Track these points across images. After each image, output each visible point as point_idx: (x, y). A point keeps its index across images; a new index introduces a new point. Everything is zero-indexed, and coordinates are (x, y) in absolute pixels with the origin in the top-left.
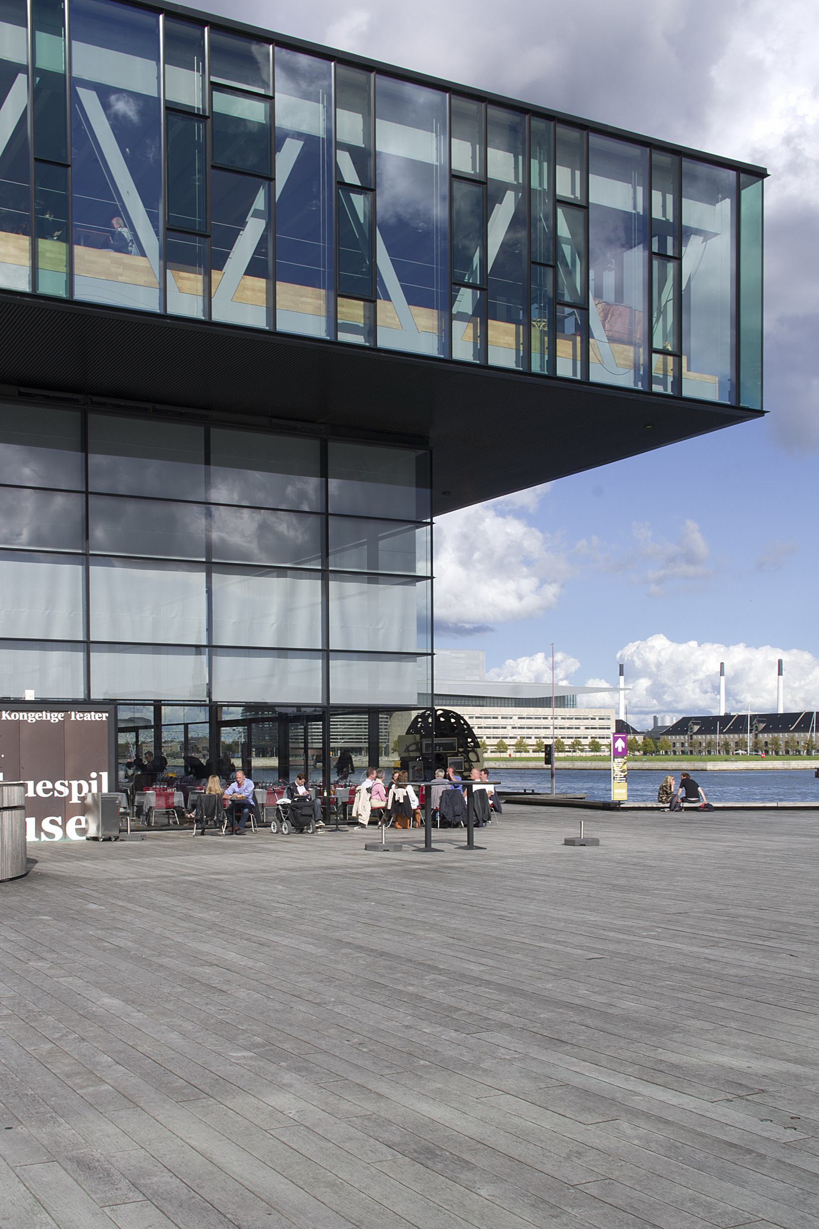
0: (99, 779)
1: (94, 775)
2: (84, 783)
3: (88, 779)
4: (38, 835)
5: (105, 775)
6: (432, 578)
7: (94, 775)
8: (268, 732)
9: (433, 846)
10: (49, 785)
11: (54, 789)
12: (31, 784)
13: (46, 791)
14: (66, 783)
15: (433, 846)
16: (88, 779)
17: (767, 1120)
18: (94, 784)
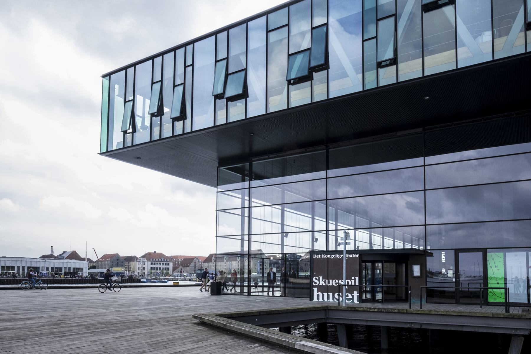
0: (355, 280)
1: (353, 278)
2: (349, 281)
3: (351, 279)
4: (333, 300)
5: (357, 278)
6: (217, 210)
7: (353, 278)
8: (120, 263)
9: (252, 294)
10: (337, 281)
11: (339, 283)
12: (331, 281)
13: (336, 283)
14: (318, 278)
15: (252, 294)
16: (351, 279)
17: (63, 254)
18: (353, 281)
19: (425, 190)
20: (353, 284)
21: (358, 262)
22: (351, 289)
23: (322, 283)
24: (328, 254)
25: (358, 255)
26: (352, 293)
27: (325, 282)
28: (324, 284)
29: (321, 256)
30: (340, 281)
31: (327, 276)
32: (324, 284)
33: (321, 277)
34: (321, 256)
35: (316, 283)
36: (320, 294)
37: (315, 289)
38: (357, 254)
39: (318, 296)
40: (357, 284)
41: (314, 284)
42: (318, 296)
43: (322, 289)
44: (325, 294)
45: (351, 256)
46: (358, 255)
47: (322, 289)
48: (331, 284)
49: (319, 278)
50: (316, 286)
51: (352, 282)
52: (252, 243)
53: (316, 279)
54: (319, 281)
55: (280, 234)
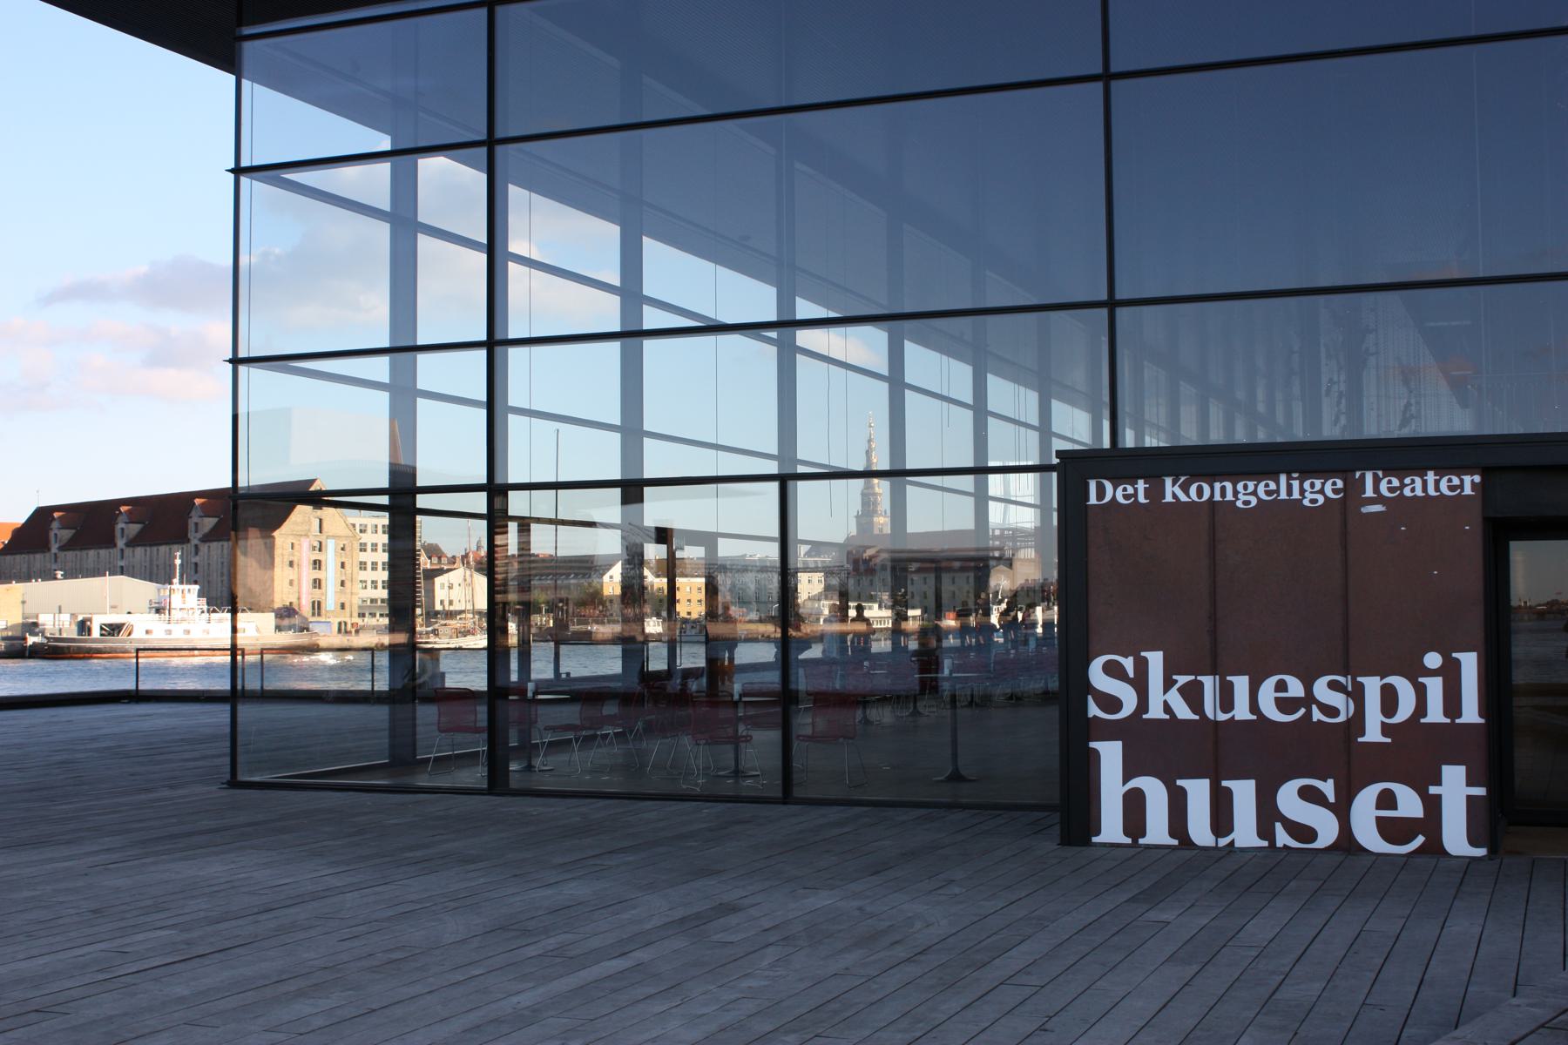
0: (1451, 673)
1: (1433, 660)
3: (1415, 672)
4: (1265, 831)
5: (1469, 663)
6: (238, 171)
7: (1433, 660)
10: (1296, 688)
11: (1309, 699)
12: (1241, 683)
14: (1128, 664)
16: (1415, 672)
18: (1435, 686)
19: (1112, 304)
20: (1435, 714)
21: (1471, 527)
22: (1415, 754)
23: (1166, 702)
24: (1211, 477)
25: (1469, 482)
26: (1425, 780)
27: (1193, 695)
28: (1183, 712)
29: (1155, 492)
30: (1321, 689)
31: (1201, 654)
32: (1183, 712)
33: (1155, 659)
34: (1155, 492)
35: (1112, 704)
36: (1154, 790)
37: (1110, 754)
38: (1460, 470)
39: (1134, 805)
40: (1471, 713)
41: (1094, 710)
42: (1134, 805)
43: (1155, 748)
44: (1198, 791)
45: (1415, 487)
46: (1469, 482)
47: (1155, 748)
48: (1242, 712)
49: (1142, 666)
50: (1110, 731)
51: (1421, 692)
52: (516, 427)
53: (1113, 670)
54: (1140, 684)
55: (240, 615)
